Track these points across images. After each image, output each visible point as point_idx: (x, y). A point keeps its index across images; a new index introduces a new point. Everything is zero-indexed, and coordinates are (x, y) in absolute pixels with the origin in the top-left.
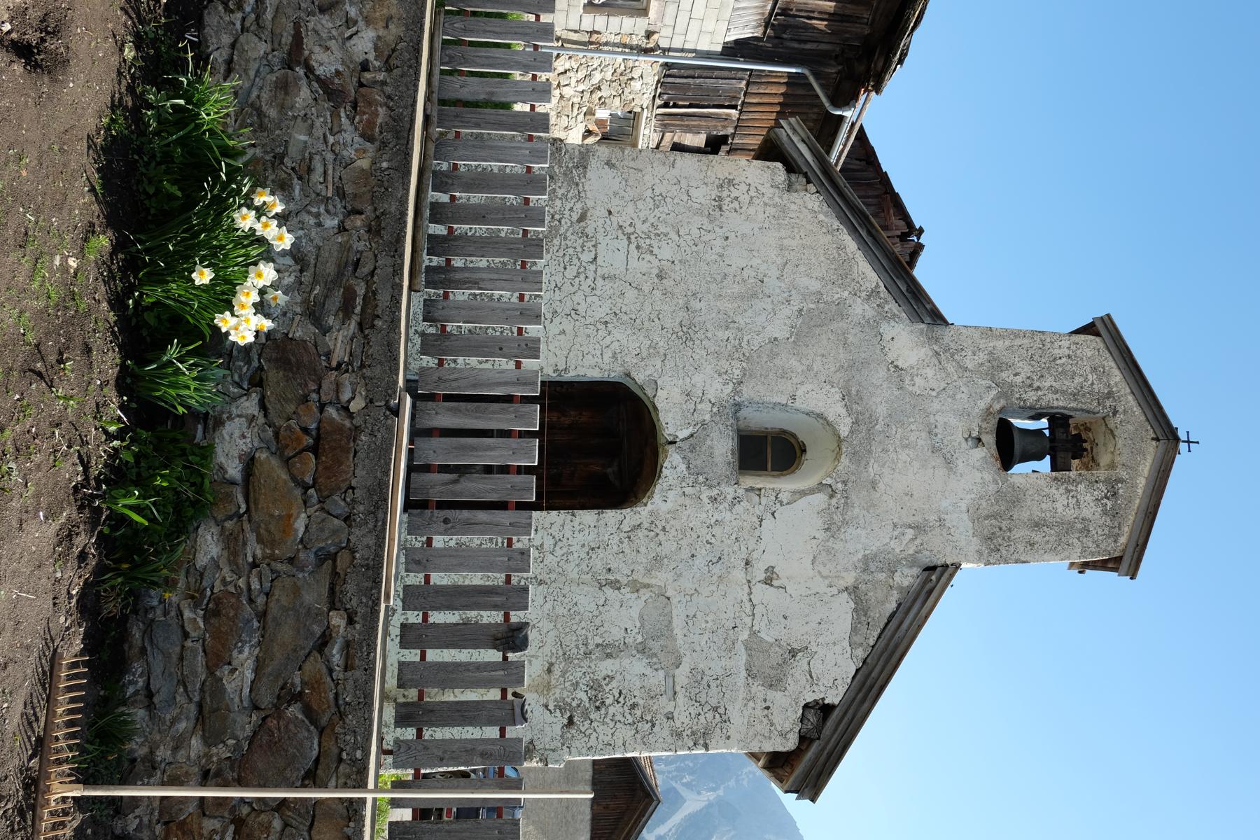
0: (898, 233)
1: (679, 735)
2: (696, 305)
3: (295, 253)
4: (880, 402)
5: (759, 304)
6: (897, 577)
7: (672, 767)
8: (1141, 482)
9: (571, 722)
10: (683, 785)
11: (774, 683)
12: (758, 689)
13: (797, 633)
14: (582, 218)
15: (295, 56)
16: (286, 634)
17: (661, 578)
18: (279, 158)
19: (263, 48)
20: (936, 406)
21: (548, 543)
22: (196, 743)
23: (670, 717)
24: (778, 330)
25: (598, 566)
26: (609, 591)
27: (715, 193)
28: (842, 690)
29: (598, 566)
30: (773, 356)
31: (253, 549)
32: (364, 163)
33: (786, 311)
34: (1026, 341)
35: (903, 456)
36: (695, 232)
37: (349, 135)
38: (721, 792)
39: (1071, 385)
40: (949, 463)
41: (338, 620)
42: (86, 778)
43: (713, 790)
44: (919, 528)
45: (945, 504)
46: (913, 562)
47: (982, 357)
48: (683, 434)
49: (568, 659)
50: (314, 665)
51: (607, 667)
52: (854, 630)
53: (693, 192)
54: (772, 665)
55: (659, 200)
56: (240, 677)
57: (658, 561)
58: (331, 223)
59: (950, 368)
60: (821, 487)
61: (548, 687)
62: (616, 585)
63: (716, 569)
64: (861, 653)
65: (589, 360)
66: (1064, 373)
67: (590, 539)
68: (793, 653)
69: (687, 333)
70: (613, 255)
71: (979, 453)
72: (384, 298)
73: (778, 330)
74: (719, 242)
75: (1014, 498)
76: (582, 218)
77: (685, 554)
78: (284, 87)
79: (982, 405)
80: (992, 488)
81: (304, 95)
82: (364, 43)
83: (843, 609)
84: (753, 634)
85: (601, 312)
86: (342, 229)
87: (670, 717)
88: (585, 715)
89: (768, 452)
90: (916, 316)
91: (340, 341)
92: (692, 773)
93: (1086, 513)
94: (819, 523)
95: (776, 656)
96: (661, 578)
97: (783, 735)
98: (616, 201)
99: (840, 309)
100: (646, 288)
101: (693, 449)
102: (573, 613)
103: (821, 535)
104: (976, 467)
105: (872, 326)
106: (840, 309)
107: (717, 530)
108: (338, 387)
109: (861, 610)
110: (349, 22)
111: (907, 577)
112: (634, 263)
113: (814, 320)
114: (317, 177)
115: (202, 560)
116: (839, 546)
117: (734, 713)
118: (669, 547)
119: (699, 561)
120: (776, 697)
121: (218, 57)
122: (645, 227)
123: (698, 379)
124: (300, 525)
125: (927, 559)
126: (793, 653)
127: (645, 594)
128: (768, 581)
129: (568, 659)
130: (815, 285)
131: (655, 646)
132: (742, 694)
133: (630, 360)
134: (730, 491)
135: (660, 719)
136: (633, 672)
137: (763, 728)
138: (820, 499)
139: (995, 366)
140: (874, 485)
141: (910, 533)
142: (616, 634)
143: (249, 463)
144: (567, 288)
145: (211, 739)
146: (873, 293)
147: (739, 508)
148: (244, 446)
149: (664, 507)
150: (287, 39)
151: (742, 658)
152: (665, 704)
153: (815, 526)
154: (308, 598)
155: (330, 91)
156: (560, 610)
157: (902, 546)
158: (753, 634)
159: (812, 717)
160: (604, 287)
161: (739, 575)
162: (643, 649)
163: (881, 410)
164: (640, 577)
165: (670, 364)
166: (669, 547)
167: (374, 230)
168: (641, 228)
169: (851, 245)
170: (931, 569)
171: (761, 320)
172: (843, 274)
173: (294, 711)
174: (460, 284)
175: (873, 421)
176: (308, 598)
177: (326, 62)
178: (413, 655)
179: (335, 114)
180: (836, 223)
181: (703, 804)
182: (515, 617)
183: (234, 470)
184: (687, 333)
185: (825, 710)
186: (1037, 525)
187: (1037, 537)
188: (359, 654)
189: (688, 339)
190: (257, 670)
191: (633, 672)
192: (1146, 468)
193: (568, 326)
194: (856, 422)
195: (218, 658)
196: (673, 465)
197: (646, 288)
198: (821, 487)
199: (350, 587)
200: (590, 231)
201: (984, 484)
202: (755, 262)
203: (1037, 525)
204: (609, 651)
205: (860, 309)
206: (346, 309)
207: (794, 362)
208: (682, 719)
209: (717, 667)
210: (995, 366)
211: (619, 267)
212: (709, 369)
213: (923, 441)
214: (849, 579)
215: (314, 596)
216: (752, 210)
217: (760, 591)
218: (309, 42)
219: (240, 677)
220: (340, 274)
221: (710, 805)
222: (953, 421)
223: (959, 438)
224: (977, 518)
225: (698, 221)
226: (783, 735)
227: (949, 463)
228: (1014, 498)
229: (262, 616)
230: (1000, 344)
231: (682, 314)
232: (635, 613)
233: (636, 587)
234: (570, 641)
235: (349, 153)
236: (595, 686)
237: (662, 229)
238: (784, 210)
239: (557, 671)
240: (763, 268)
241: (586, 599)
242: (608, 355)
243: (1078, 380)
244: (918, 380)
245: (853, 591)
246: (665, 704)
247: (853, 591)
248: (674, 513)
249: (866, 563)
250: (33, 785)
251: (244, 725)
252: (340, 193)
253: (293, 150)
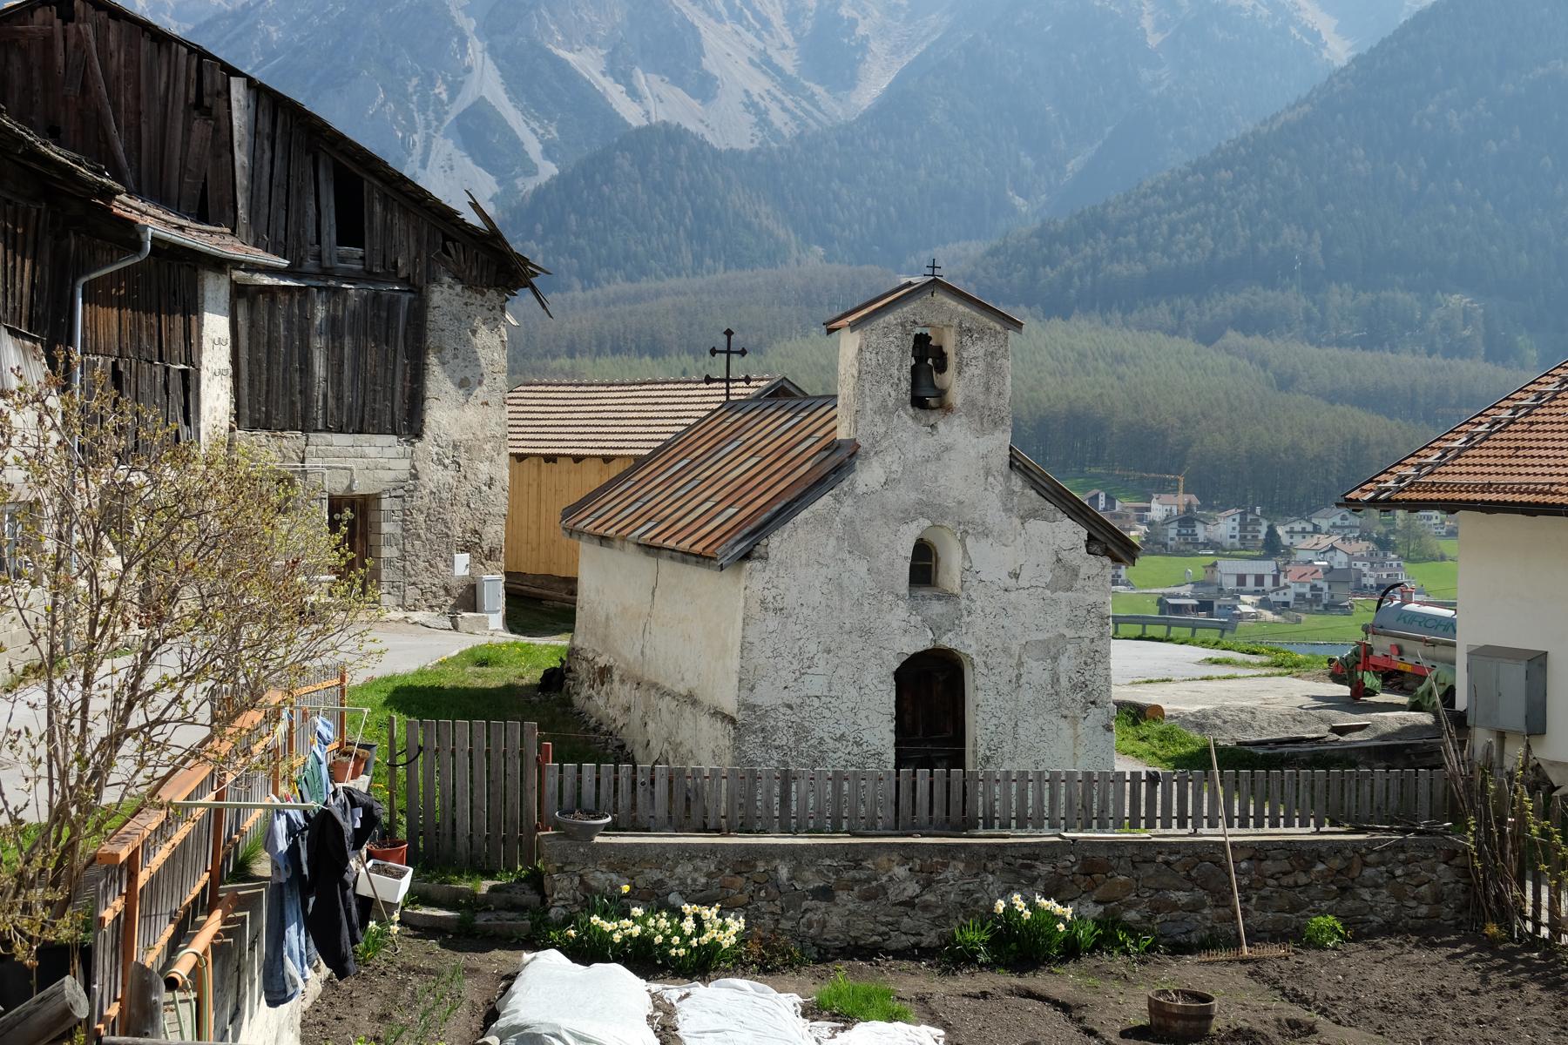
0: (58, 23)
1: (1102, 635)
2: (848, 626)
3: (1001, 897)
4: (907, 496)
5: (846, 582)
6: (1017, 489)
7: (419, 118)
8: (961, 308)
9: (1093, 703)
10: (452, 98)
11: (1075, 573)
12: (1079, 584)
13: (1047, 558)
14: (790, 707)
15: (910, 903)
16: (1166, 880)
17: (1015, 648)
18: (963, 905)
19: (906, 919)
20: (910, 456)
21: (994, 721)
22: (1206, 911)
23: (1092, 641)
24: (861, 568)
25: (1007, 689)
26: (1022, 681)
27: (771, 614)
28: (1080, 528)
29: (1007, 689)
30: (879, 572)
31: (1132, 897)
32: (961, 866)
33: (850, 562)
34: (867, 386)
35: (942, 481)
36: (798, 627)
37: (948, 874)
38: (469, 25)
39: (897, 354)
40: (947, 449)
41: (1160, 859)
42: (1240, 944)
43: (463, 41)
44: (988, 473)
45: (973, 453)
46: (1008, 478)
47: (877, 419)
48: (931, 636)
49: (1059, 706)
50: (1177, 867)
51: (1064, 681)
52: (1046, 519)
53: (770, 629)
54: (1066, 575)
55: (776, 654)
56: (1181, 897)
57: (1006, 650)
58: (991, 878)
59: (885, 444)
60: (962, 541)
61: (1074, 717)
62: (1019, 676)
63: (1010, 611)
64: (1059, 515)
65: (885, 699)
66: (888, 358)
67: (992, 694)
68: (1059, 560)
69: (866, 632)
70: (815, 685)
71: (941, 427)
72: (1026, 851)
73: (861, 568)
74: (804, 609)
75: (971, 403)
76: (790, 707)
77: (1002, 632)
78: (926, 907)
79: (910, 422)
80: (964, 419)
81: (930, 897)
82: (901, 872)
83: (1034, 526)
84: (1047, 587)
85: (853, 692)
86: (993, 873)
87: (1092, 641)
88: (1090, 693)
89: (923, 566)
90: (851, 469)
91: (1043, 869)
92: (430, 80)
93: (981, 353)
94: (983, 541)
95: (1060, 572)
96: (1015, 648)
97: (1104, 567)
98: (777, 683)
99: (849, 523)
100: (837, 661)
101: (939, 628)
102: (1033, 703)
103: (990, 540)
104: (954, 431)
105: (858, 499)
106: (849, 523)
107: (988, 611)
108: (1065, 868)
109: (1034, 514)
110: (891, 879)
111: (1017, 482)
112: (820, 670)
113: (856, 544)
114: (971, 887)
115: (1138, 917)
116: (997, 529)
117: (1091, 599)
118: (998, 643)
119: (1006, 623)
120: (1083, 572)
121: (913, 940)
122: (795, 663)
123: (895, 624)
124: (1122, 878)
125: (1006, 468)
126: (1059, 560)
127: (1025, 658)
128: (1017, 576)
129: (1059, 706)
130: (832, 542)
131: (1053, 650)
132: (1081, 594)
133: (885, 671)
134: (964, 602)
135: (1093, 647)
136: (1066, 664)
137: (1099, 581)
138: (969, 541)
139: (883, 409)
140: (960, 503)
141: (990, 479)
142: (1046, 676)
143: (1097, 902)
144: (837, 716)
145: (1204, 905)
146: (836, 498)
147: (974, 596)
148: (1091, 905)
149: (974, 647)
150: (902, 909)
151: (1060, 594)
152: (1085, 644)
153: (985, 544)
154: (1151, 872)
155: (927, 885)
156: (1032, 712)
157: (998, 484)
158: (1047, 587)
159: (1094, 548)
160: (837, 688)
161: (1013, 596)
162: (1055, 659)
163: (914, 496)
164: (1014, 662)
165: (886, 644)
166: (998, 643)
167: (993, 857)
168: (796, 666)
169: (804, 514)
170: (1011, 465)
171: (856, 581)
172: (824, 520)
173: (1193, 874)
174: (993, 811)
175: (920, 502)
176: (1151, 872)
177: (912, 889)
178: (1158, 822)
179: (939, 882)
180: (789, 525)
181: (489, 63)
182: (1144, 777)
183: (1101, 908)
184: (866, 632)
185: (1091, 539)
186: (988, 389)
187: (995, 389)
188: (1173, 848)
189: (869, 631)
190: (1178, 890)
191: (1066, 664)
192: (951, 303)
193: (862, 714)
194: (922, 514)
195: (1174, 906)
196: (948, 641)
197: (837, 661)
198: (962, 541)
199: (1148, 854)
200: (799, 701)
201: (960, 425)
202: (817, 584)
203: (988, 389)
204: (1055, 680)
205: (847, 509)
206: (1030, 867)
207: (883, 557)
208: (1094, 633)
209: (1066, 610)
210: (883, 409)
211: (823, 680)
212: (889, 617)
213: (932, 467)
214: (1017, 521)
215: (1150, 869)
216: (782, 587)
217: (1023, 582)
218: (902, 898)
219: (1181, 897)
220: (1012, 871)
221: (492, 50)
222: (920, 444)
223: (930, 440)
224: (981, 432)
225: (790, 626)
226: (1104, 567)
227: (947, 449)
228: (971, 403)
229: (1157, 890)
230: (869, 405)
231: (853, 636)
232: (1035, 664)
233: (1020, 664)
234: (1049, 704)
235: (957, 872)
236: (1074, 688)
237: (796, 651)
238: (780, 563)
239: (1066, 712)
240: (821, 579)
241: (1027, 695)
242: (881, 686)
243: (893, 349)
244: (894, 467)
245: (1024, 519)
246: (1085, 644)
247: (1024, 519)
248: (978, 640)
249: (1007, 510)
250: (1244, 962)
251: (1199, 893)
252: (976, 875)
253: (959, 899)
